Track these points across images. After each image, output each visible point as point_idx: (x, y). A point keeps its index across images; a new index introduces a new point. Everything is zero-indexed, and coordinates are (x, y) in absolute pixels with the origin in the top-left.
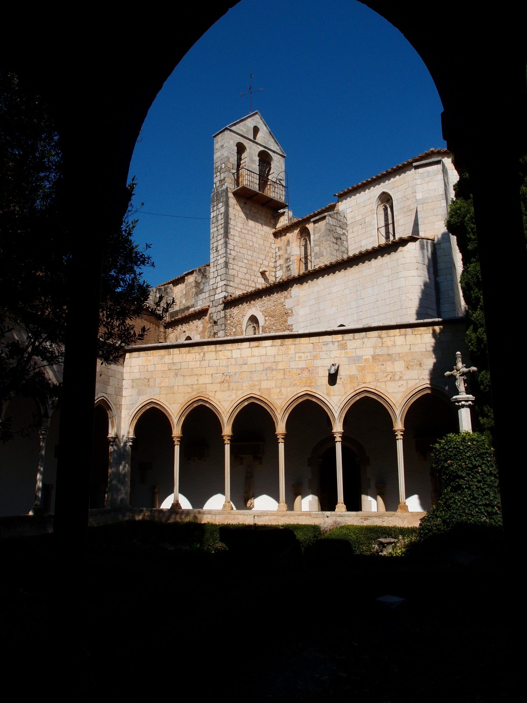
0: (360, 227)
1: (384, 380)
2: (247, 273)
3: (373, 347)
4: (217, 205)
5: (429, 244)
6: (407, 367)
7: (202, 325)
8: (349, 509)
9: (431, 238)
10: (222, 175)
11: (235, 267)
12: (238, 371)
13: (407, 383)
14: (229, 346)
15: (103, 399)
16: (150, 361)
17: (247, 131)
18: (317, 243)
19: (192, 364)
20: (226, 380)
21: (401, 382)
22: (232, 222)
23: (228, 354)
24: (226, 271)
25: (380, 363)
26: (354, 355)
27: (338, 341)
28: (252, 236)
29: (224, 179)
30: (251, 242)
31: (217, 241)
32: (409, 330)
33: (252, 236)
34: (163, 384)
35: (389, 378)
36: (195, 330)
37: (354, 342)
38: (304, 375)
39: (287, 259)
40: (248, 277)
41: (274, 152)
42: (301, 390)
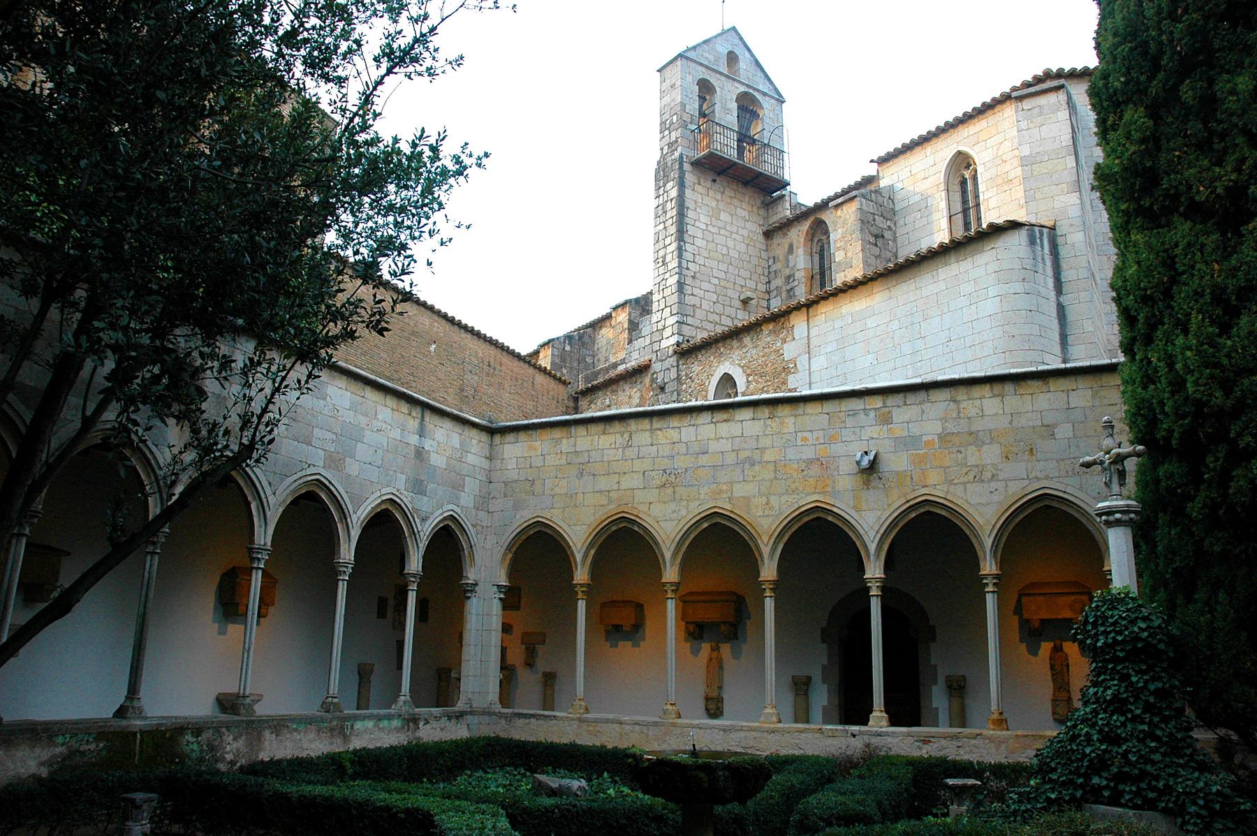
1: (962, 480)
3: (941, 419)
7: (638, 394)
8: (893, 722)
9: (1050, 224)
11: (696, 291)
14: (674, 422)
19: (610, 454)
20: (670, 481)
21: (993, 485)
22: (690, 214)
23: (673, 434)
25: (955, 450)
26: (905, 433)
31: (665, 247)
32: (1009, 388)
34: (557, 490)
35: (971, 477)
36: (628, 400)
37: (904, 413)
38: (811, 473)
39: (789, 277)
40: (719, 308)
41: (765, 94)
42: (807, 500)
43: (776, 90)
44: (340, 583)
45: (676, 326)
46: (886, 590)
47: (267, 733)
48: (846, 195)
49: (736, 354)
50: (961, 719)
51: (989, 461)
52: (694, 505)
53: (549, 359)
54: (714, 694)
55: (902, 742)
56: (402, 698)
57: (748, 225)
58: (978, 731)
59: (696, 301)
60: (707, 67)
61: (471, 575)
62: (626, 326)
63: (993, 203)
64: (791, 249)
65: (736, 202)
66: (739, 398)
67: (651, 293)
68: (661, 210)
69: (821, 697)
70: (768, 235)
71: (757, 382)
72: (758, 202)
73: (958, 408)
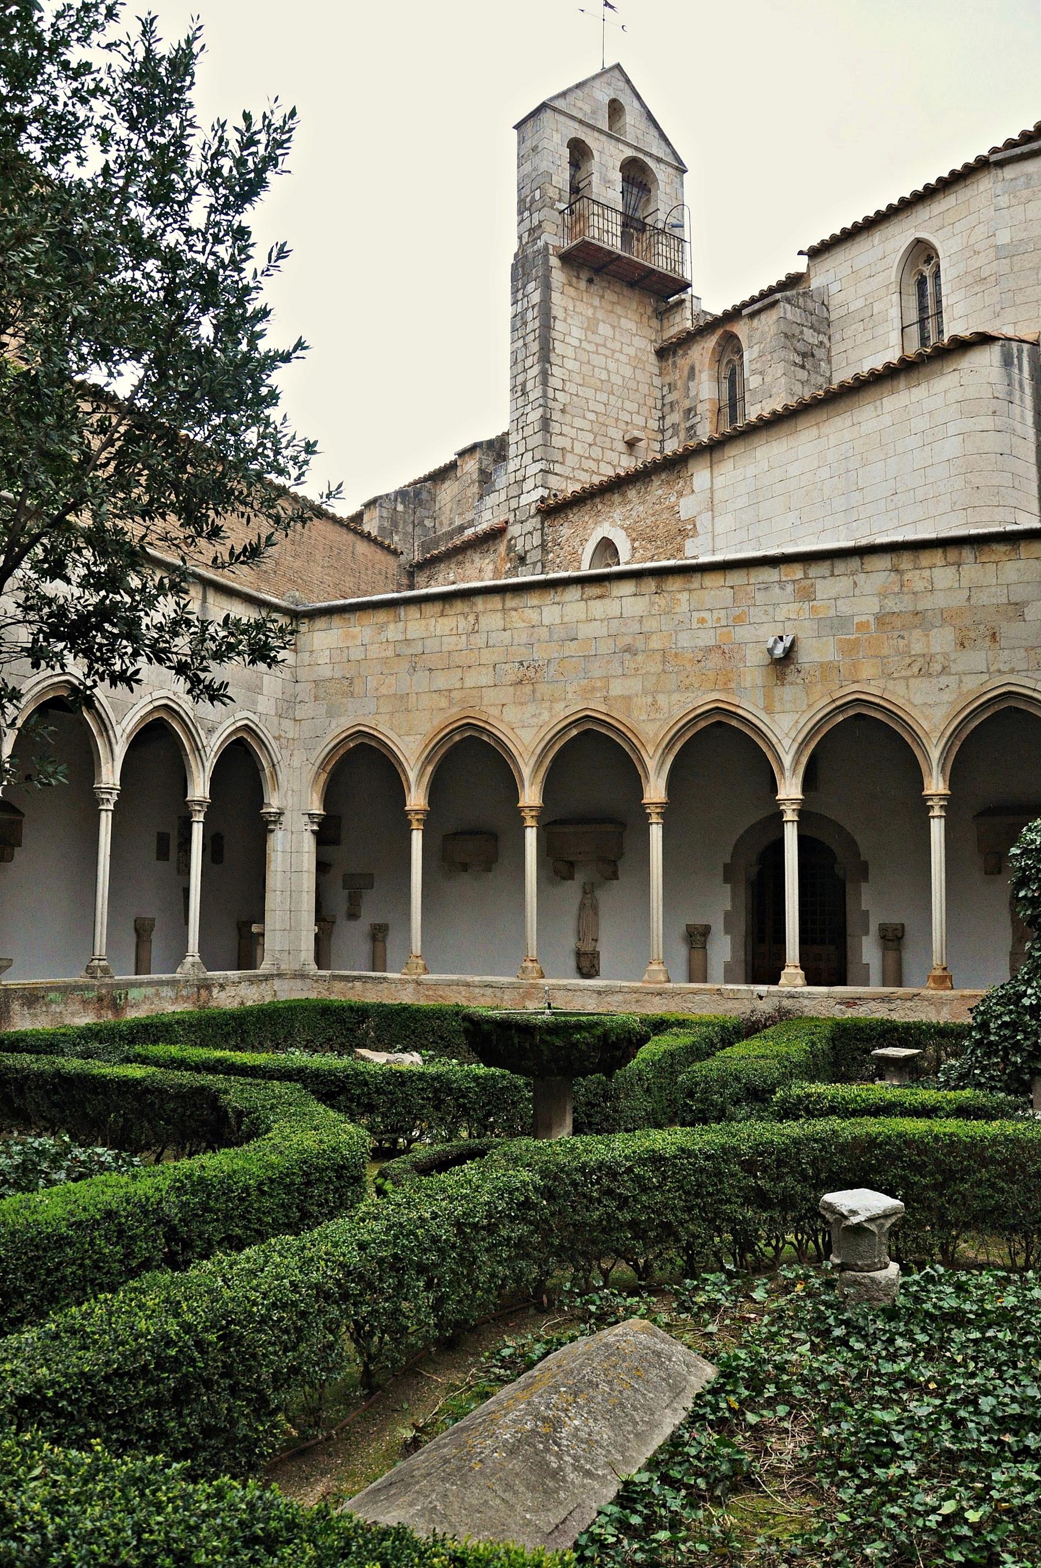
0: (860, 326)
1: (903, 673)
2: (595, 444)
3: (879, 594)
4: (524, 287)
5: (1025, 354)
6: (962, 644)
7: (491, 567)
8: (810, 981)
10: (535, 215)
11: (566, 430)
12: (556, 655)
13: (961, 681)
14: (533, 599)
15: (246, 725)
16: (354, 637)
17: (594, 112)
18: (758, 365)
19: (450, 643)
20: (527, 679)
21: (944, 680)
22: (559, 325)
23: (533, 615)
24: (545, 440)
25: (896, 634)
26: (832, 613)
27: (794, 581)
28: (607, 357)
29: (540, 226)
30: (605, 372)
31: (525, 370)
32: (967, 554)
33: (607, 357)
34: (384, 691)
35: (916, 670)
37: (830, 586)
38: (710, 665)
39: (689, 410)
40: (596, 453)
41: (659, 160)
42: (703, 699)
43: (674, 153)
44: (103, 814)
45: (540, 476)
46: (805, 817)
47: (16, 1006)
48: (765, 301)
49: (618, 513)
50: (895, 976)
51: (939, 650)
52: (559, 706)
53: (376, 523)
54: (589, 948)
55: (824, 1002)
56: (189, 959)
57: (636, 340)
58: (915, 991)
59: (566, 443)
60: (581, 122)
61: (273, 801)
62: (475, 476)
63: (959, 310)
64: (692, 373)
65: (619, 310)
66: (622, 567)
67: (508, 434)
68: (518, 321)
69: (723, 949)
70: (662, 353)
71: (645, 549)
72: (649, 311)
73: (901, 581)
